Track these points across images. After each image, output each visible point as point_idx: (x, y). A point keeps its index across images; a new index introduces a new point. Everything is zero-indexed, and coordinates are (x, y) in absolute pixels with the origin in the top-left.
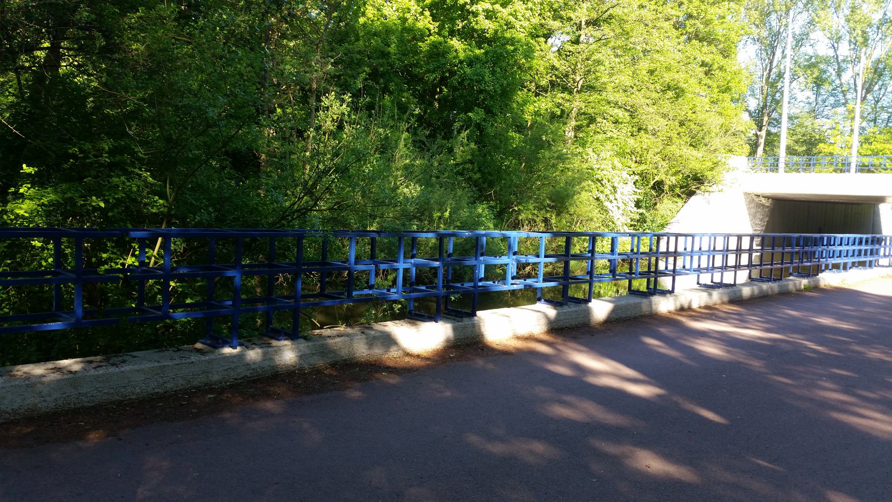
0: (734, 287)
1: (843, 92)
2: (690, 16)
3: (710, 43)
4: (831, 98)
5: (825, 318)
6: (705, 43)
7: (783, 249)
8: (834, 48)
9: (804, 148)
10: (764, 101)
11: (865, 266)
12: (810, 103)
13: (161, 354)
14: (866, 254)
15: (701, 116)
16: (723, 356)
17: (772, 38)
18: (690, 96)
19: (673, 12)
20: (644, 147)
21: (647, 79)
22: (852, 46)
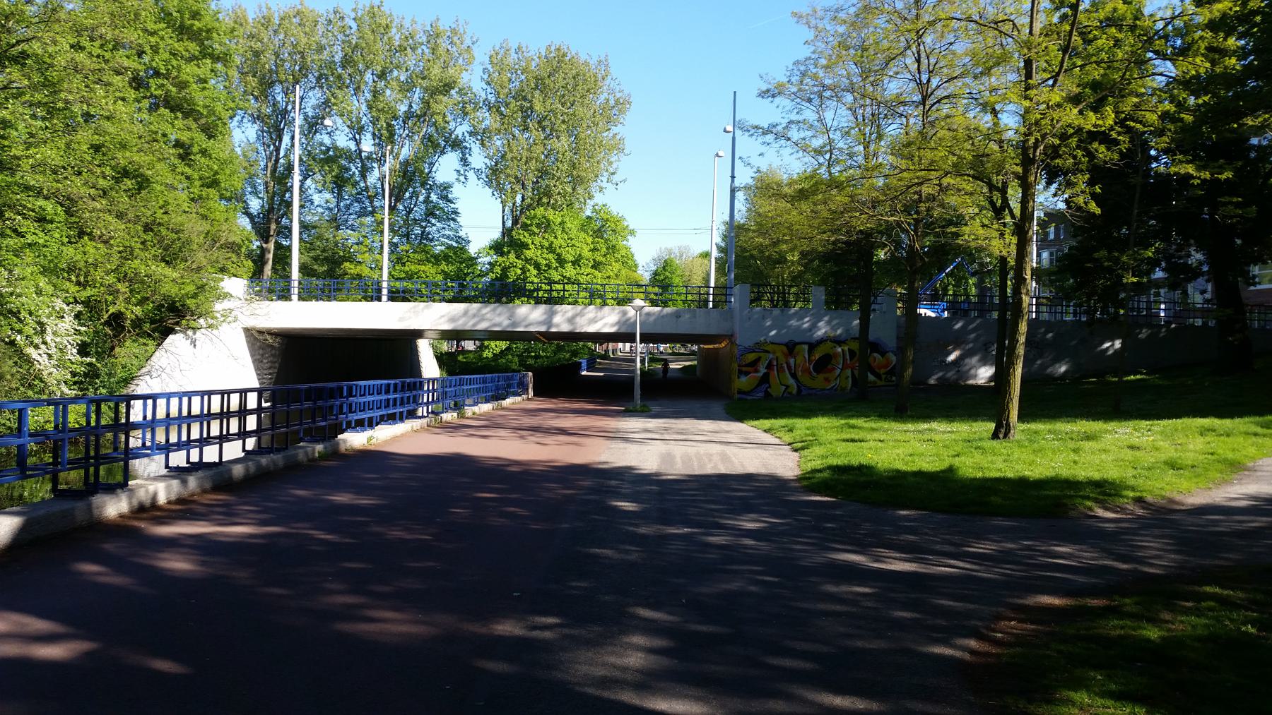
0: (220, 467)
1: (369, 197)
2: (157, 74)
3: (187, 115)
4: (356, 204)
5: (344, 494)
6: (179, 115)
7: (288, 406)
8: (356, 140)
9: (325, 268)
10: (270, 202)
11: (395, 419)
12: (330, 209)
13: (1021, 474)
14: (395, 405)
15: (176, 219)
16: (190, 571)
17: (277, 117)
18: (159, 188)
19: (126, 63)
20: (90, 261)
21: (90, 159)
22: (377, 141)
